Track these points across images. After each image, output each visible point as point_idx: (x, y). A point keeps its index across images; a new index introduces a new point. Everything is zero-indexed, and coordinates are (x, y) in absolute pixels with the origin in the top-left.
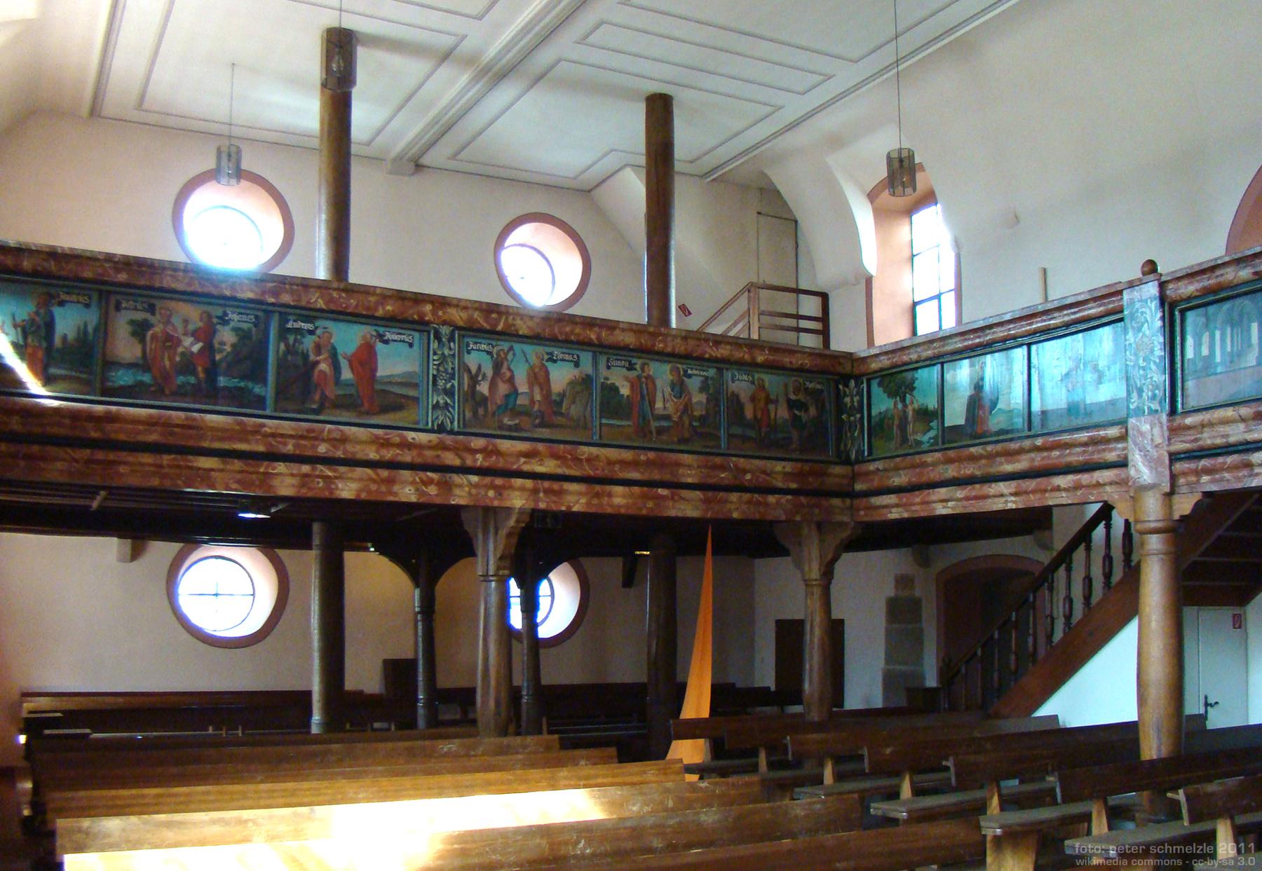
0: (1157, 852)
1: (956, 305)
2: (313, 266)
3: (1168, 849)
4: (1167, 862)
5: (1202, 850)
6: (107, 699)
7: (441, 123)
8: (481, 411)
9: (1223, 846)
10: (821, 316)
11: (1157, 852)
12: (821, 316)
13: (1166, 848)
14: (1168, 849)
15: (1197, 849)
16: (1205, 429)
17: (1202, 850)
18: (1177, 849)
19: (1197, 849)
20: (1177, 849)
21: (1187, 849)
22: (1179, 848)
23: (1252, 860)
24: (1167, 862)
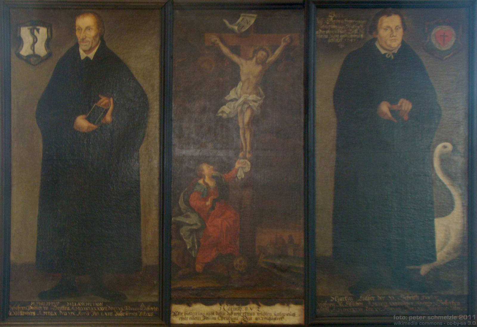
5: (451, 318)
9: (421, 318)
17: (451, 318)
21: (413, 318)
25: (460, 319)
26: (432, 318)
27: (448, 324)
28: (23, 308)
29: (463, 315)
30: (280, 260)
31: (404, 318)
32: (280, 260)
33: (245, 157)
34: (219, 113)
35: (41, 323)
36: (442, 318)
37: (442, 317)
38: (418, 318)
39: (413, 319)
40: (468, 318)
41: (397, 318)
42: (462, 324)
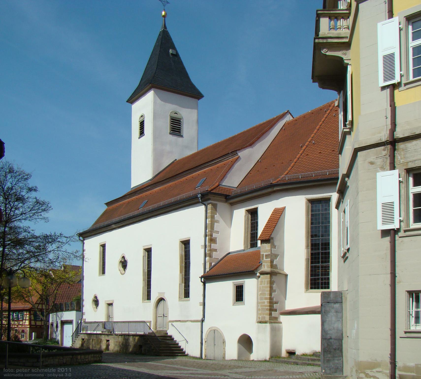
0: (34, 372)
1: (99, 265)
2: (268, 261)
3: (39, 370)
4: (38, 375)
5: (51, 371)
6: (97, 233)
7: (371, 371)
8: (33, 256)
9: (59, 369)
10: (226, 359)
11: (34, 372)
12: (226, 359)
13: (38, 370)
14: (39, 370)
15: (49, 370)
16: (52, 278)
17: (51, 371)
18: (42, 370)
19: (49, 370)
20: (42, 370)
21: (45, 370)
22: (42, 370)
23: (70, 374)
24: (38, 375)
25: (58, 371)
26: (36, 370)
27: (49, 375)
28: (5, 326)
29: (19, 370)
30: (79, 237)
31: (12, 370)
32: (79, 237)
33: (27, 182)
34: (7, 248)
35: (182, 354)
36: (43, 371)
37: (43, 370)
38: (24, 370)
39: (19, 372)
40: (65, 370)
41: (7, 370)
42: (60, 375)
